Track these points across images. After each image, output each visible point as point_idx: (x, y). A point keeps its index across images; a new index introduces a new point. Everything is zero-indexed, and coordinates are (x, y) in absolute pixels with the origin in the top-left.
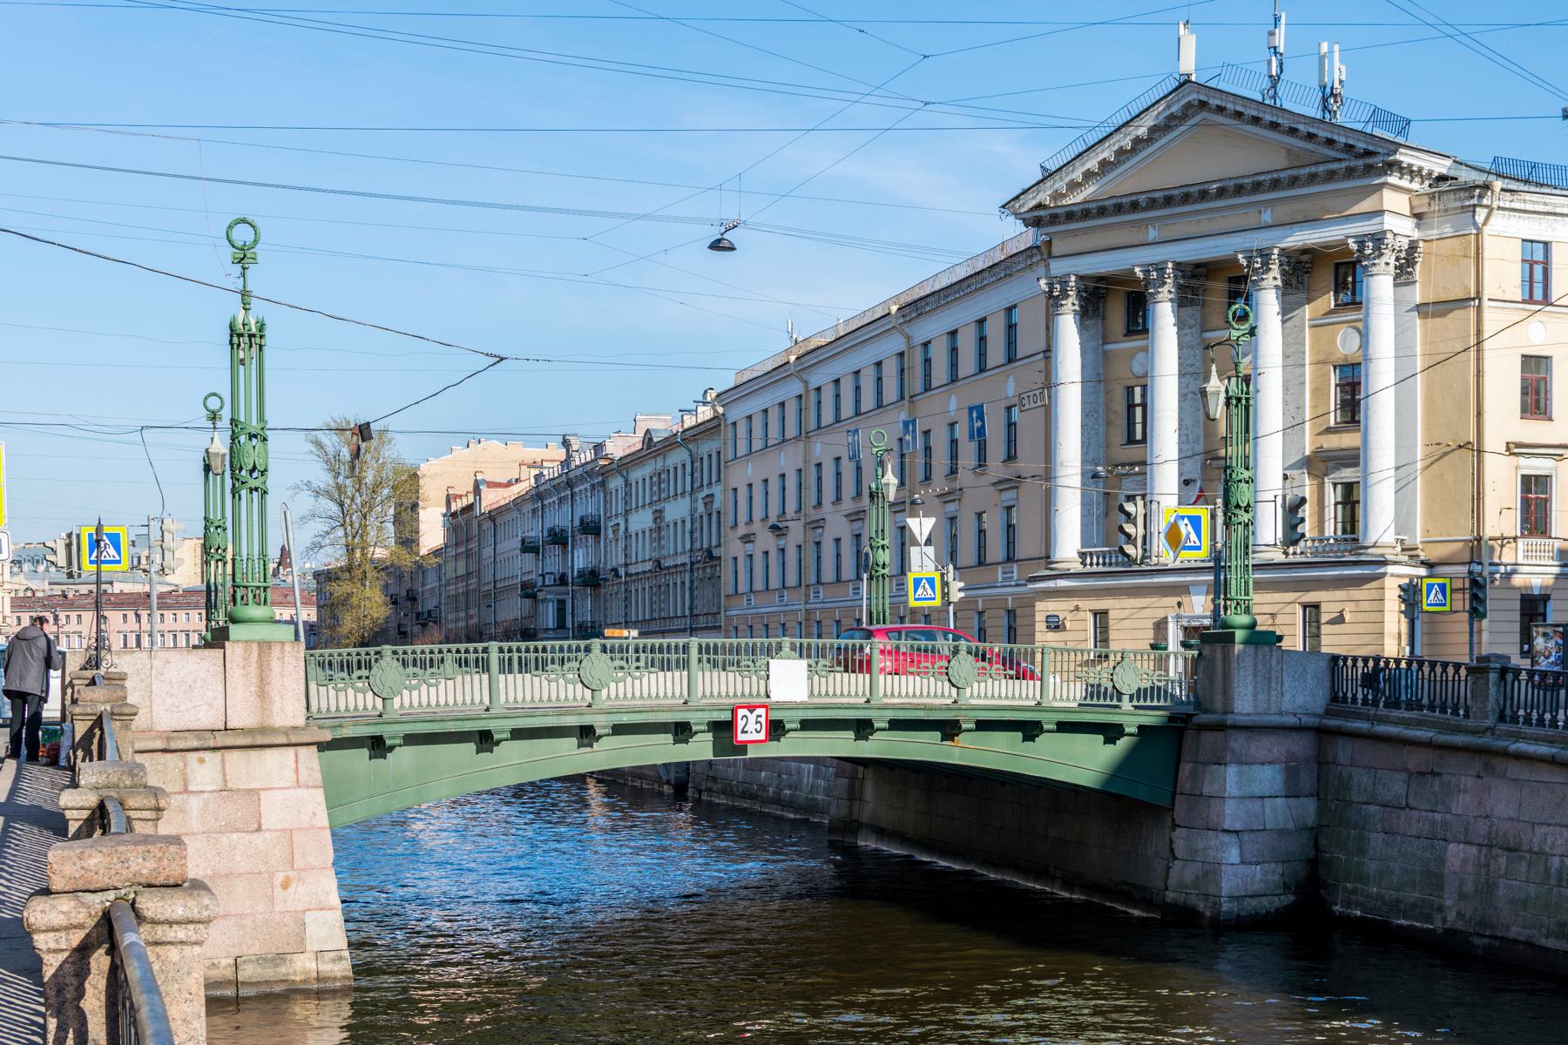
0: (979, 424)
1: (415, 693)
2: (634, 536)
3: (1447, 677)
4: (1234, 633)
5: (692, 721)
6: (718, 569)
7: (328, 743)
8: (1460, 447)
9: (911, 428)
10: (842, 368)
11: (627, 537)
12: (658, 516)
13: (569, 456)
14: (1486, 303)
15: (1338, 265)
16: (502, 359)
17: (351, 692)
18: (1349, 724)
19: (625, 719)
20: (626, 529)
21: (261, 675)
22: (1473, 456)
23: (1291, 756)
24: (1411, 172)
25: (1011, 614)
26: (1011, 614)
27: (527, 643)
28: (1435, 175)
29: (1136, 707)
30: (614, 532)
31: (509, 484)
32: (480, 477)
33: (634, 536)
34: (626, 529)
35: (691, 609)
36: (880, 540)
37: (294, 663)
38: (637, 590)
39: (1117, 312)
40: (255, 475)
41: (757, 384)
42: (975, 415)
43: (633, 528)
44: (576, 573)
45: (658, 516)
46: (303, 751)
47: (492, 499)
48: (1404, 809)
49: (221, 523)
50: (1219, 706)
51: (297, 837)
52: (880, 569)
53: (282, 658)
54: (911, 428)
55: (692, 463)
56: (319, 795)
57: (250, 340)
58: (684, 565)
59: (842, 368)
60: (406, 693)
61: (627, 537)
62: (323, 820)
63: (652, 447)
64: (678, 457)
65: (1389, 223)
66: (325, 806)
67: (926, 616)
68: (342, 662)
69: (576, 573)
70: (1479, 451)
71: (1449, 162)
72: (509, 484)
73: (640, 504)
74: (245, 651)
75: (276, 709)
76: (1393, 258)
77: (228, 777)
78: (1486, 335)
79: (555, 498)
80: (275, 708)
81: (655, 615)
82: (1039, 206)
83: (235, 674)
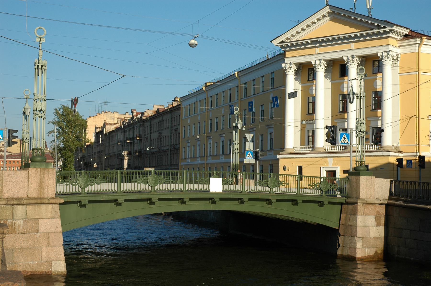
0: (277, 102)
1: (93, 186)
2: (152, 140)
3: (424, 187)
4: (359, 172)
5: (215, 198)
6: (178, 151)
7: (63, 203)
8: (412, 117)
9: (251, 104)
10: (218, 90)
11: (151, 140)
12: (160, 134)
13: (133, 116)
14: (421, 73)
15: (373, 61)
16: (124, 76)
17: (71, 186)
18: (391, 202)
19: (306, 199)
20: (150, 138)
21: (41, 179)
22: (416, 120)
23: (378, 213)
24: (397, 33)
25: (271, 166)
26: (271, 166)
27: (136, 171)
28: (404, 34)
29: (328, 196)
30: (146, 139)
31: (114, 124)
32: (96, 126)
33: (152, 140)
34: (150, 138)
35: (170, 163)
36: (236, 141)
37: (52, 176)
38: (153, 157)
39: (306, 73)
40: (41, 112)
41: (185, 98)
42: (275, 100)
43: (152, 138)
44: (134, 151)
45: (160, 134)
46: (54, 205)
47: (108, 129)
48: (419, 231)
49: (28, 131)
50: (354, 196)
51: (50, 235)
52: (236, 150)
53: (48, 174)
54: (251, 104)
55: (171, 118)
56: (59, 221)
57: (41, 67)
58: (168, 149)
59: (218, 90)
60: (89, 186)
61: (151, 140)
62: (60, 229)
63: (159, 114)
64: (166, 117)
65: (390, 48)
66: (61, 224)
67: (244, 166)
68: (65, 176)
69: (134, 151)
70: (419, 118)
71: (409, 31)
72: (114, 124)
73: (155, 131)
74: (36, 171)
75: (45, 191)
76: (392, 59)
77: (28, 214)
78: (420, 84)
79: (138, 125)
80: (45, 191)
81: (159, 165)
82: (282, 42)
83: (32, 179)
